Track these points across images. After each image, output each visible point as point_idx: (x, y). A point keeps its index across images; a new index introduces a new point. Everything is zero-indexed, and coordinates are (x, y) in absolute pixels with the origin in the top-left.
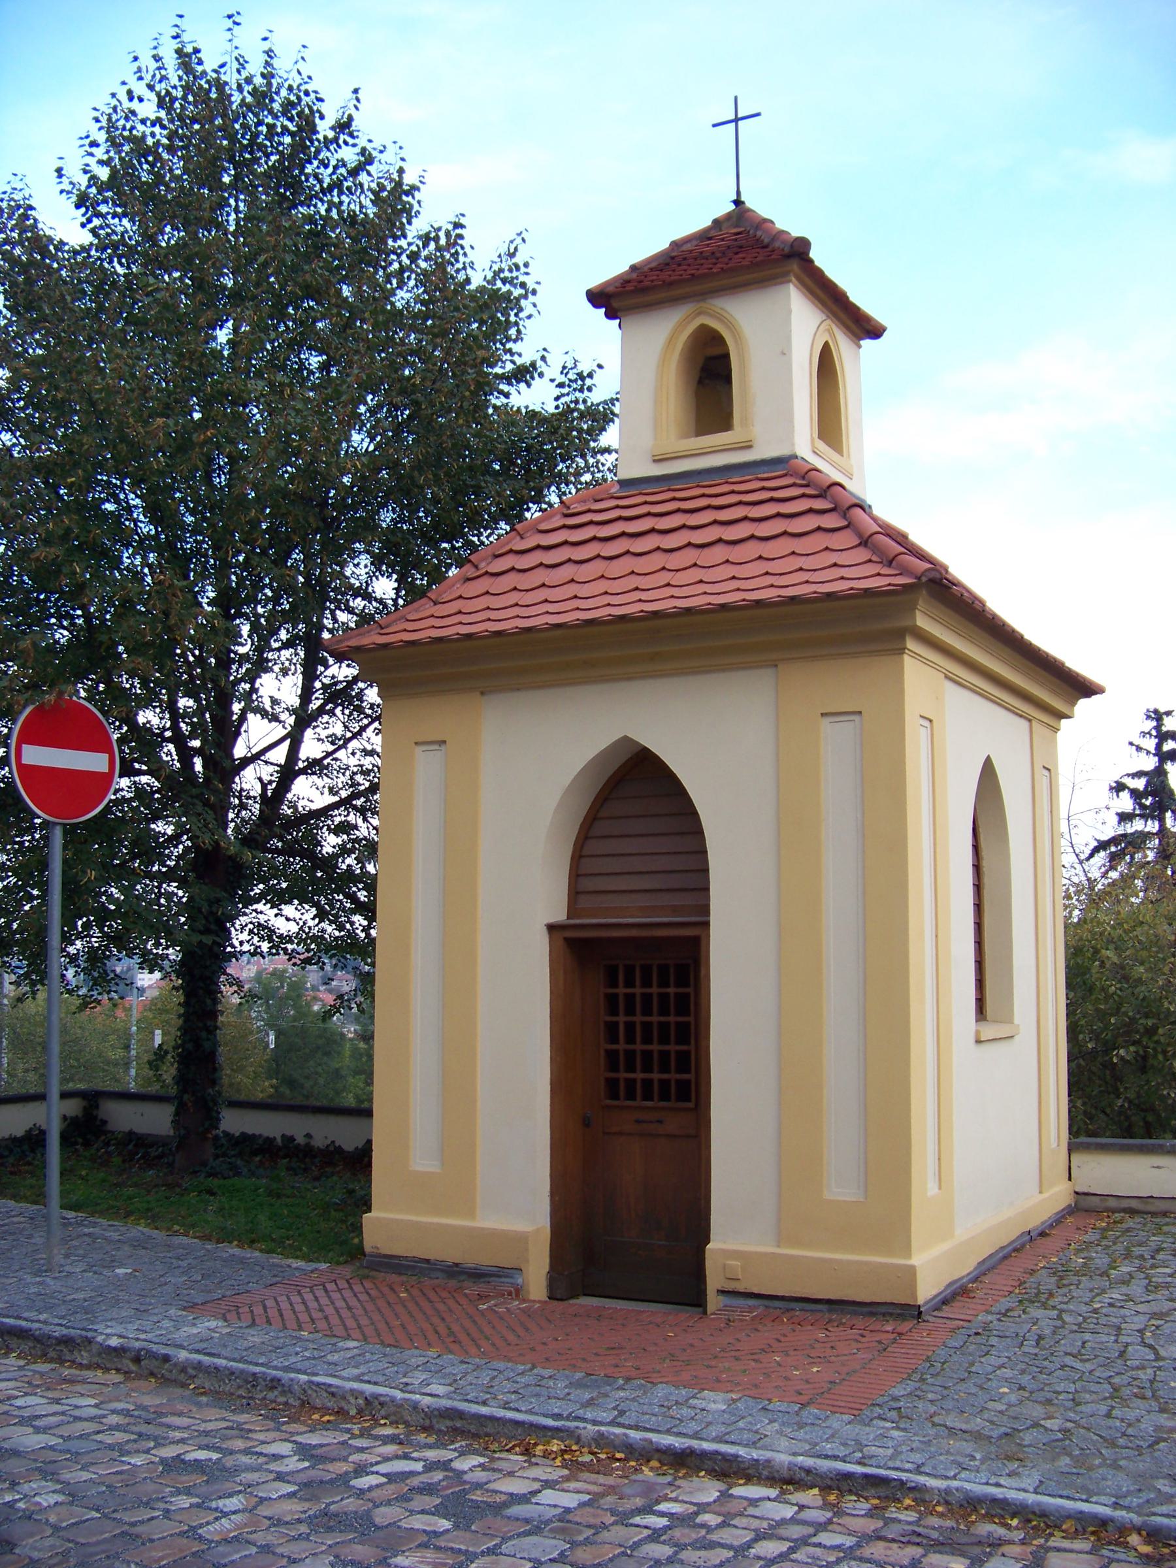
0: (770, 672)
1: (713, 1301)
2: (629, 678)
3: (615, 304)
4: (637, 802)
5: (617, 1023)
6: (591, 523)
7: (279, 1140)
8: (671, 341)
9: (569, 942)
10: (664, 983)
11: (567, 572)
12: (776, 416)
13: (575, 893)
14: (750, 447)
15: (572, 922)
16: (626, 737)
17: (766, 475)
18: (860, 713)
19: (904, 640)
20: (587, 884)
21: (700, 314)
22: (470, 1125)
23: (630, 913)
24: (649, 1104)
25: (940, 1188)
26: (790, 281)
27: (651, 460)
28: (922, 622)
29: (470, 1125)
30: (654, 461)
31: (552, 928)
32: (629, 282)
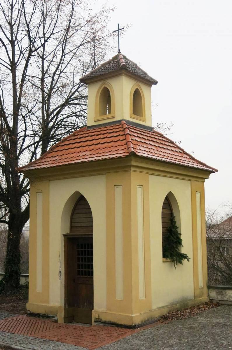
0: (104, 176)
1: (94, 324)
2: (60, 179)
3: (86, 82)
4: (79, 206)
5: (79, 257)
6: (114, 132)
7: (183, 259)
8: (98, 91)
9: (68, 238)
10: (85, 248)
11: (106, 145)
12: (122, 110)
13: (71, 227)
14: (114, 118)
15: (71, 234)
16: (77, 191)
17: (105, 127)
18: (122, 185)
19: (130, 168)
20: (73, 225)
21: (104, 84)
22: (47, 282)
23: (81, 233)
24: (86, 276)
25: (145, 298)
26: (123, 75)
27: (94, 121)
28: (133, 163)
29: (47, 282)
30: (95, 121)
31: (64, 235)
32: (89, 76)
